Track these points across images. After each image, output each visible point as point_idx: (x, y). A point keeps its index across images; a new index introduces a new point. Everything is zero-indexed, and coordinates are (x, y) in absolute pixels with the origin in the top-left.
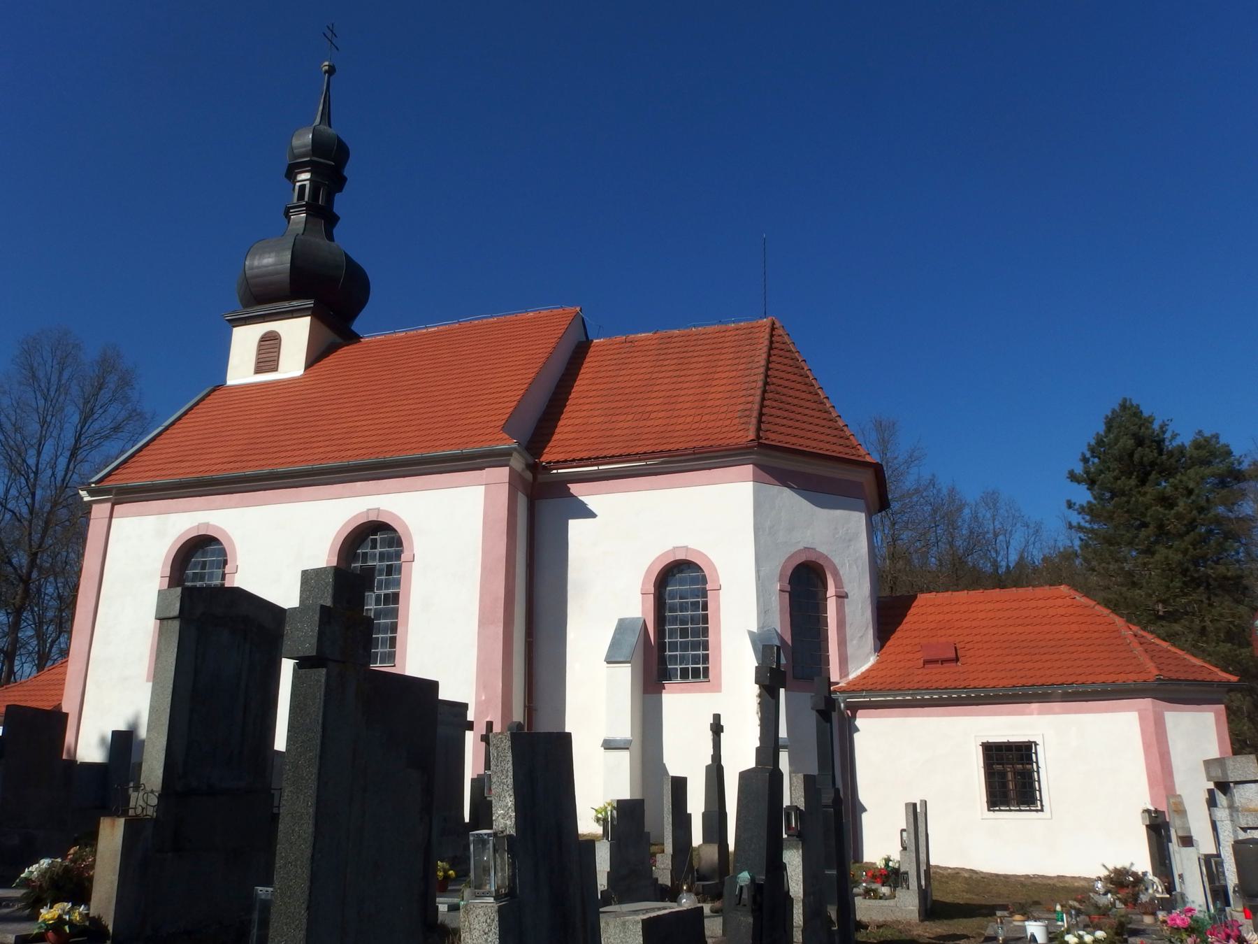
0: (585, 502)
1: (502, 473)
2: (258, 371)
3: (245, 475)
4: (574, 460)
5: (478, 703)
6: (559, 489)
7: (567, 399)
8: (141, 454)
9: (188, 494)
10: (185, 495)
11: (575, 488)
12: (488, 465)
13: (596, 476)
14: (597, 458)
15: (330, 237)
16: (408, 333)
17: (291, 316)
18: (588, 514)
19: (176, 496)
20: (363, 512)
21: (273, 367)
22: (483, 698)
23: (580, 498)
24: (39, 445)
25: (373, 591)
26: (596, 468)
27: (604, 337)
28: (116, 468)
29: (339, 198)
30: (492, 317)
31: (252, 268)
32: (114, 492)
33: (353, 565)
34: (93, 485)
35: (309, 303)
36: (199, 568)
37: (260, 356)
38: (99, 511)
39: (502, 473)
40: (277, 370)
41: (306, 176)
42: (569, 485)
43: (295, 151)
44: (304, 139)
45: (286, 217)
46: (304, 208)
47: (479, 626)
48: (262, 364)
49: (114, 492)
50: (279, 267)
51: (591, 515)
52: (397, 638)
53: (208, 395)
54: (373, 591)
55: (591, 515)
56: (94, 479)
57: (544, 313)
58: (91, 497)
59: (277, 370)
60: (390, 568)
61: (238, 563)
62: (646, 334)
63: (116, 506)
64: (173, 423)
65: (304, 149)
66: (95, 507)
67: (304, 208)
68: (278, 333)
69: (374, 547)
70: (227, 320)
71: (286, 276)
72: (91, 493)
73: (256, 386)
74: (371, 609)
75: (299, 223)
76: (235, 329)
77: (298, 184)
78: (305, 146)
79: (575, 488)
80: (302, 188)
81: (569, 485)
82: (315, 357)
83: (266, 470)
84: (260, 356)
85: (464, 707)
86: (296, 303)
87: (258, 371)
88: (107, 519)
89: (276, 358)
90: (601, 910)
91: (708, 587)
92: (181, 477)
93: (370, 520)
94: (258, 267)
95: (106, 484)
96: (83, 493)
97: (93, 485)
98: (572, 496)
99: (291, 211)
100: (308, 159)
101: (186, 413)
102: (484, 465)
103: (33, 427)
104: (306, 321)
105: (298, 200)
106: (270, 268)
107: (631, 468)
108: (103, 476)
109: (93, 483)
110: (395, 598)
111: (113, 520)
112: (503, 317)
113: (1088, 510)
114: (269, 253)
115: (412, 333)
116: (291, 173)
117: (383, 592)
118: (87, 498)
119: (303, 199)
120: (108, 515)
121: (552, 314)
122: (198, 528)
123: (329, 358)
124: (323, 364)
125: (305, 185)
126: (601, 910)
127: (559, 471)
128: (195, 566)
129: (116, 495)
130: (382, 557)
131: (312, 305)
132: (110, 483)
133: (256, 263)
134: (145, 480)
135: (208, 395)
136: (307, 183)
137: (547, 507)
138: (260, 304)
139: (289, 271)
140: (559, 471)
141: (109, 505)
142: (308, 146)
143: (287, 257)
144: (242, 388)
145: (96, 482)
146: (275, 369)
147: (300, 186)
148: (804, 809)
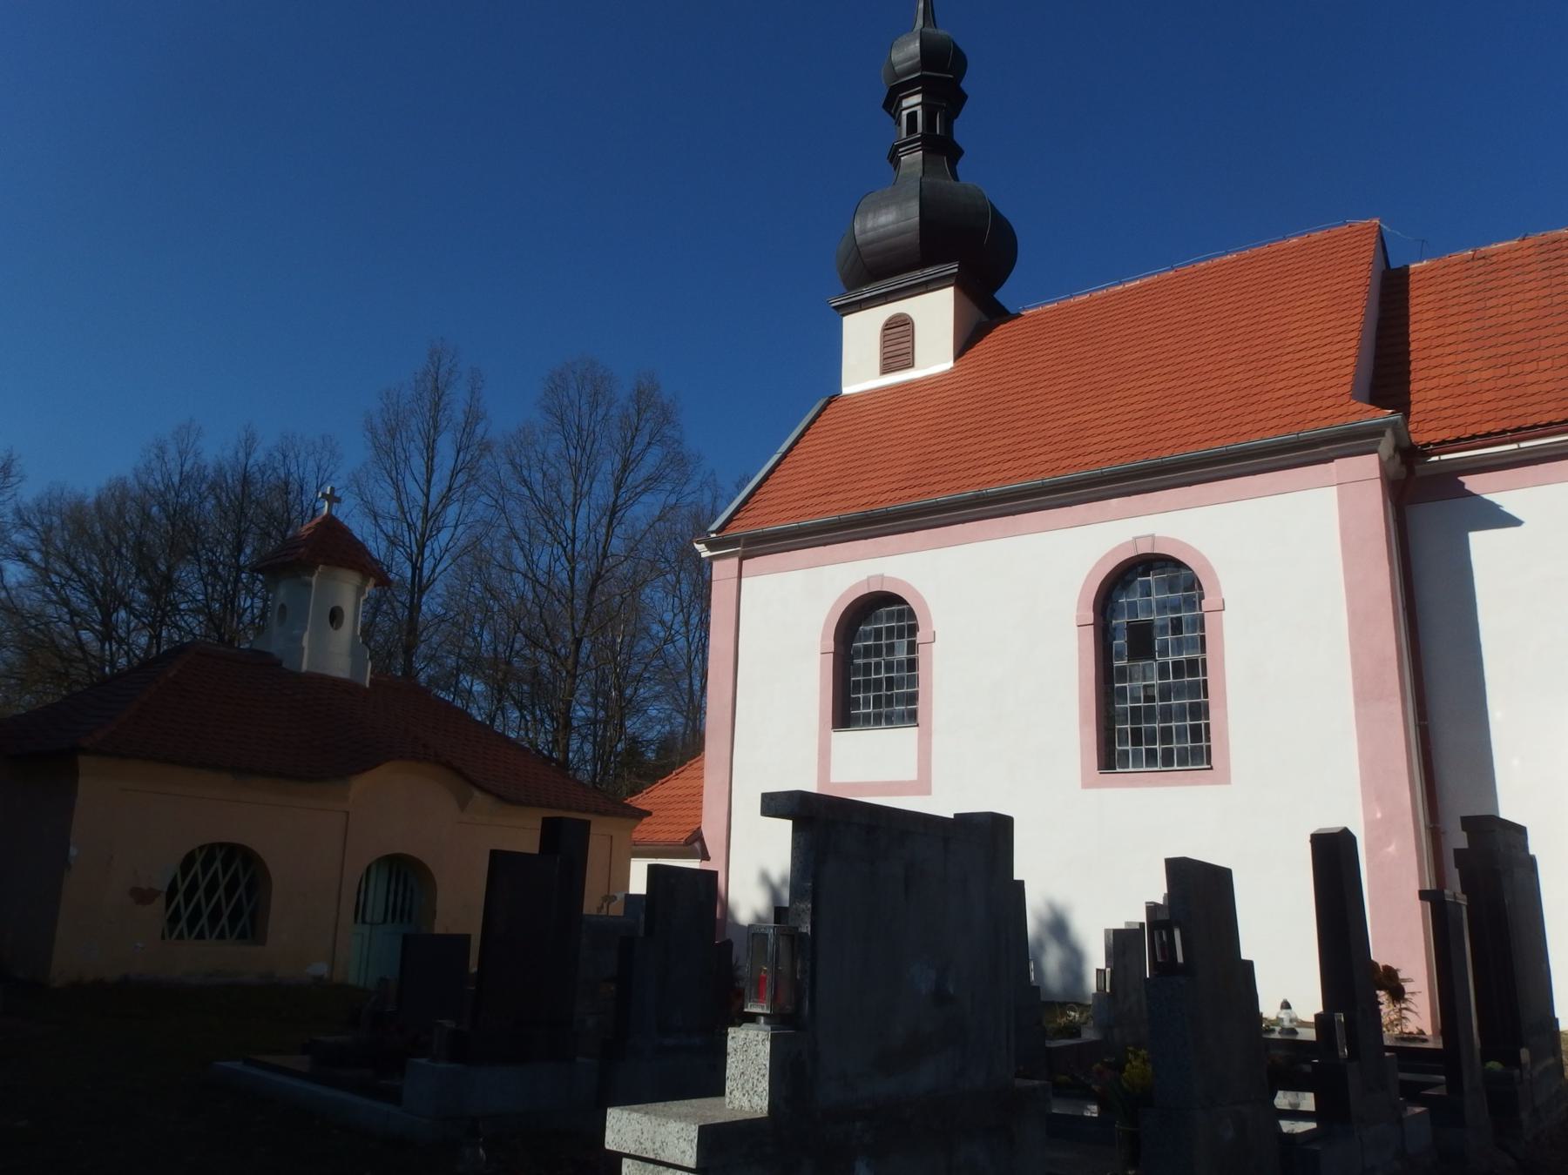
0: (1497, 503)
1: (1368, 466)
2: (886, 369)
3: (937, 502)
4: (1474, 437)
5: (1370, 825)
6: (1448, 485)
7: (1408, 353)
8: (761, 490)
9: (848, 537)
10: (833, 540)
11: (1472, 483)
12: (1336, 453)
13: (1510, 459)
14: (1519, 429)
15: (956, 178)
16: (1094, 294)
18: (1500, 519)
19: (794, 546)
20: (1127, 543)
21: (906, 362)
22: (1379, 815)
23: (1486, 497)
24: (574, 506)
25: (1153, 658)
26: (1514, 446)
27: (1427, 258)
28: (737, 511)
29: (959, 126)
30: (1227, 253)
31: (864, 232)
32: (742, 541)
33: (1114, 622)
34: (713, 535)
35: (953, 268)
36: (872, 639)
38: (723, 571)
39: (1368, 466)
41: (917, 99)
42: (1461, 478)
43: (896, 68)
44: (907, 51)
45: (891, 162)
46: (919, 143)
47: (1357, 704)
48: (890, 361)
49: (742, 541)
50: (902, 224)
51: (1511, 521)
53: (824, 408)
54: (1153, 658)
55: (1511, 521)
56: (714, 527)
57: (1317, 235)
58: (711, 551)
59: (913, 366)
60: (1177, 626)
61: (934, 629)
62: (1507, 243)
63: (744, 562)
64: (790, 449)
65: (910, 63)
66: (716, 564)
67: (919, 143)
68: (908, 316)
69: (1147, 592)
70: (834, 307)
71: (914, 236)
72: (711, 545)
73: (888, 390)
74: (1153, 685)
75: (914, 164)
76: (846, 319)
77: (905, 113)
78: (911, 58)
79: (1472, 483)
80: (912, 117)
81: (1461, 478)
82: (966, 341)
83: (970, 492)
85: (500, 861)
86: (931, 271)
87: (886, 369)
88: (736, 580)
89: (910, 350)
90: (1313, 1125)
92: (864, 509)
93: (1140, 553)
94: (874, 229)
95: (729, 533)
96: (700, 547)
97: (713, 535)
98: (1470, 494)
99: (900, 150)
100: (919, 74)
101: (802, 435)
102: (1331, 455)
103: (567, 489)
104: (948, 294)
105: (908, 134)
106: (890, 227)
107: (1560, 444)
108: (724, 523)
109: (712, 532)
110: (1195, 667)
111: (743, 580)
112: (1248, 251)
114: (887, 206)
115: (1100, 293)
116: (892, 103)
117: (1171, 659)
118: (706, 554)
120: (736, 574)
122: (869, 584)
123: (973, 350)
124: (978, 351)
125: (915, 112)
126: (1313, 1125)
127: (1444, 457)
128: (867, 636)
129: (744, 546)
130: (1163, 606)
131: (956, 270)
132: (731, 532)
133: (870, 224)
134: (825, 515)
135: (824, 408)
136: (919, 109)
137: (1426, 515)
138: (878, 281)
139: (918, 227)
140: (1444, 457)
141: (735, 560)
142: (917, 56)
143: (914, 208)
144: (868, 394)
145: (716, 532)
146: (910, 365)
147: (908, 115)
148: (1378, 992)
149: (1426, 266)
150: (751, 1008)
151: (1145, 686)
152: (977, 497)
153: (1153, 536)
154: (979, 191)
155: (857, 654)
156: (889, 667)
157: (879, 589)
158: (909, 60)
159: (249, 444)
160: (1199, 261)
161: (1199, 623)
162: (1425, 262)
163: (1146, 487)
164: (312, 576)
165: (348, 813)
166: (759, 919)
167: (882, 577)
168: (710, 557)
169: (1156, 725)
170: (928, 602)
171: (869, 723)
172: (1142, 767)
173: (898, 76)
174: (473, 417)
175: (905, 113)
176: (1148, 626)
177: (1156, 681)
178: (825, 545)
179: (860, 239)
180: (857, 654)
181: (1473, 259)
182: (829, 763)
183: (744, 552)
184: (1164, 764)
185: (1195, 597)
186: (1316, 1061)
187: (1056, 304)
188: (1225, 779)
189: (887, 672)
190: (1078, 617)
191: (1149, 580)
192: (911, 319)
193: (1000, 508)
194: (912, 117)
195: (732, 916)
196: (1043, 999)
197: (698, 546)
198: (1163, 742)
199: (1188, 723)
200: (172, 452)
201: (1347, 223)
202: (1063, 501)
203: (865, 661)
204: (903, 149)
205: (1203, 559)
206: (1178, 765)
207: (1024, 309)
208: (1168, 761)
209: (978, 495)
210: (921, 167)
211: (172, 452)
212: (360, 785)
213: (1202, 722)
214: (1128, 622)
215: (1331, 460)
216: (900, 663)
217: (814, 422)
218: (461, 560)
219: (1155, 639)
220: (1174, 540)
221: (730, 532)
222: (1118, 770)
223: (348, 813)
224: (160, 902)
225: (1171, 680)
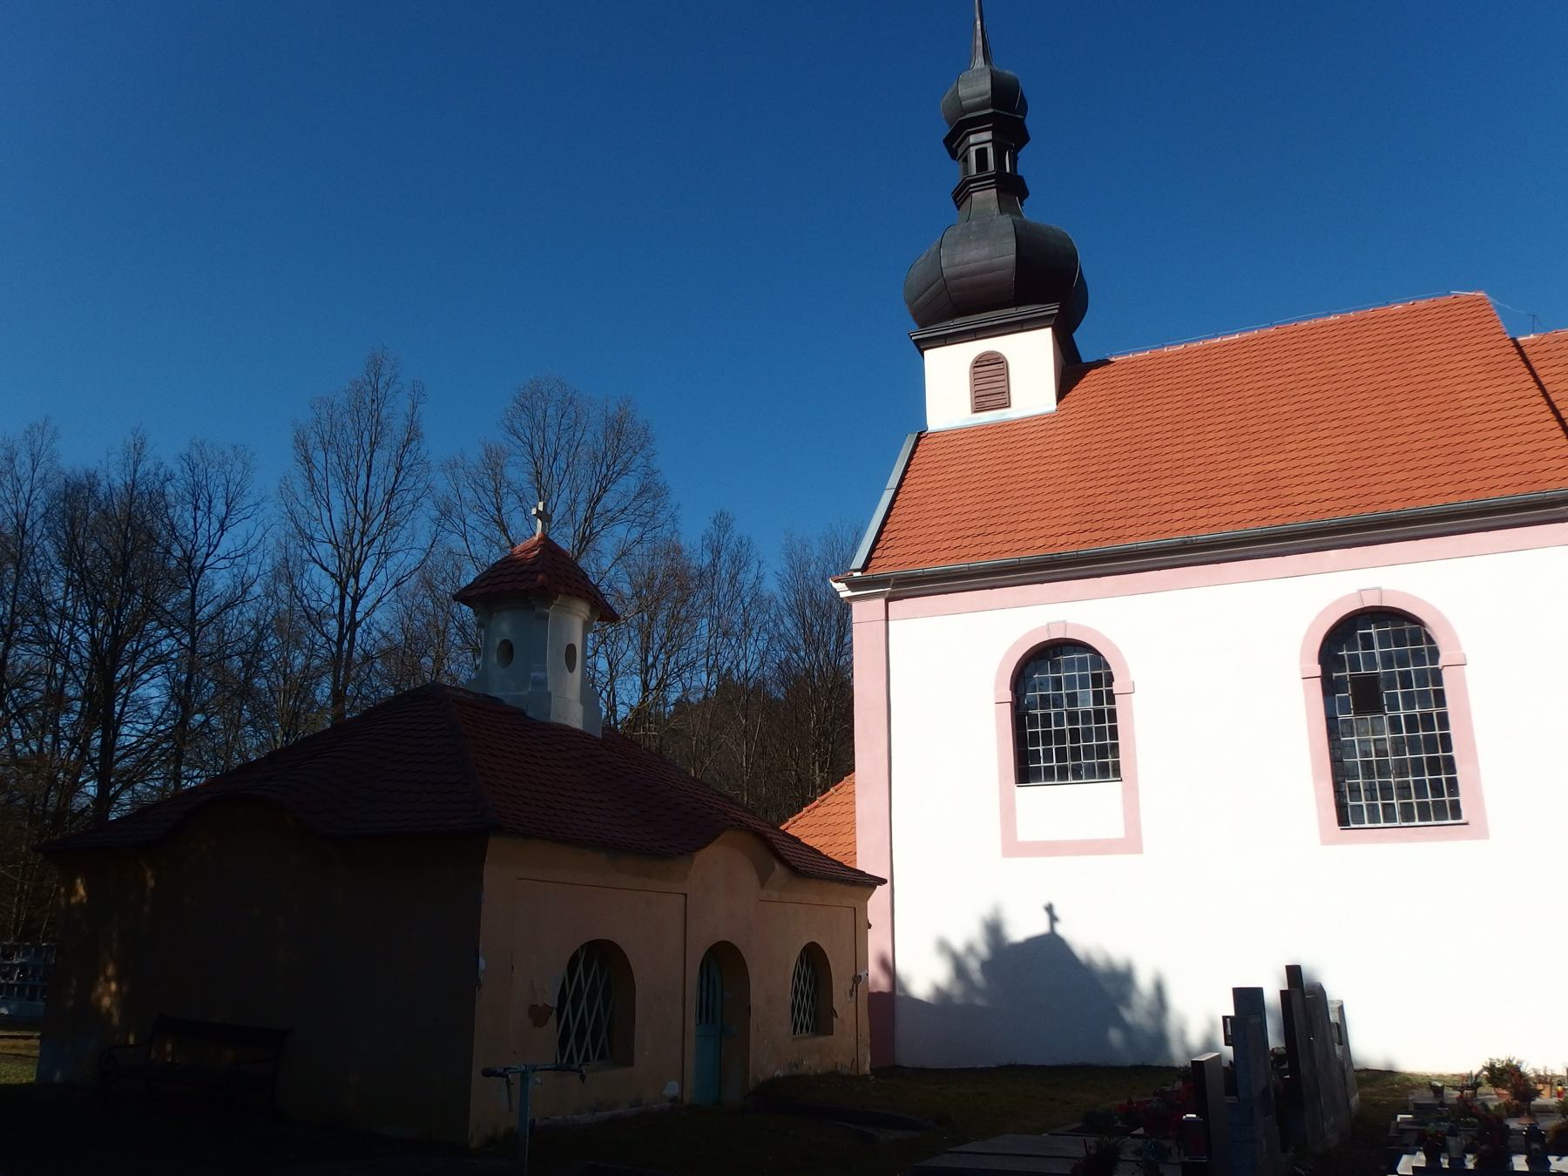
2: (978, 408)
17: (1020, 329)
21: (1002, 402)
37: (978, 388)
38: (866, 613)
40: (1009, 406)
41: (987, 136)
44: (975, 86)
46: (993, 180)
52: (1458, 779)
54: (1383, 712)
57: (1422, 304)
59: (1009, 406)
61: (1132, 678)
65: (978, 99)
66: (855, 605)
67: (993, 180)
72: (853, 584)
84: (978, 388)
87: (978, 408)
91: (1116, 688)
96: (839, 586)
99: (972, 185)
111: (890, 622)
113: (588, 617)
118: (843, 591)
119: (986, 168)
120: (884, 617)
121: (1434, 305)
129: (894, 586)
131: (1057, 311)
133: (958, 259)
141: (882, 601)
146: (1007, 405)
149: (1534, 340)
151: (1375, 740)
152: (1185, 543)
154: (1066, 234)
155: (1033, 706)
156: (1073, 718)
158: (977, 97)
159: (137, 452)
160: (1299, 320)
161: (1437, 677)
163: (1372, 539)
164: (549, 608)
165: (686, 895)
166: (938, 991)
167: (1065, 624)
168: (850, 598)
169: (1391, 780)
171: (1052, 778)
173: (966, 111)
174: (414, 433)
175: (973, 149)
176: (1374, 679)
177: (1387, 735)
178: (991, 588)
179: (947, 273)
180: (1033, 706)
182: (1014, 821)
183: (890, 593)
185: (1423, 651)
188: (1483, 834)
189: (1070, 723)
190: (1303, 670)
191: (1371, 633)
192: (1004, 358)
193: (1207, 556)
194: (981, 154)
195: (904, 989)
196: (1356, 1067)
197: (836, 586)
198: (1400, 797)
200: (24, 458)
201: (1451, 295)
202: (1276, 551)
203: (1043, 711)
204: (975, 185)
205: (1439, 613)
206: (1420, 820)
207: (1112, 356)
208: (1408, 817)
209: (1185, 542)
210: (997, 204)
211: (24, 458)
212: (703, 856)
214: (1350, 675)
216: (1086, 714)
217: (913, 459)
219: (1382, 693)
221: (875, 571)
222: (1353, 826)
223: (686, 895)
224: (553, 1019)
225: (1404, 734)
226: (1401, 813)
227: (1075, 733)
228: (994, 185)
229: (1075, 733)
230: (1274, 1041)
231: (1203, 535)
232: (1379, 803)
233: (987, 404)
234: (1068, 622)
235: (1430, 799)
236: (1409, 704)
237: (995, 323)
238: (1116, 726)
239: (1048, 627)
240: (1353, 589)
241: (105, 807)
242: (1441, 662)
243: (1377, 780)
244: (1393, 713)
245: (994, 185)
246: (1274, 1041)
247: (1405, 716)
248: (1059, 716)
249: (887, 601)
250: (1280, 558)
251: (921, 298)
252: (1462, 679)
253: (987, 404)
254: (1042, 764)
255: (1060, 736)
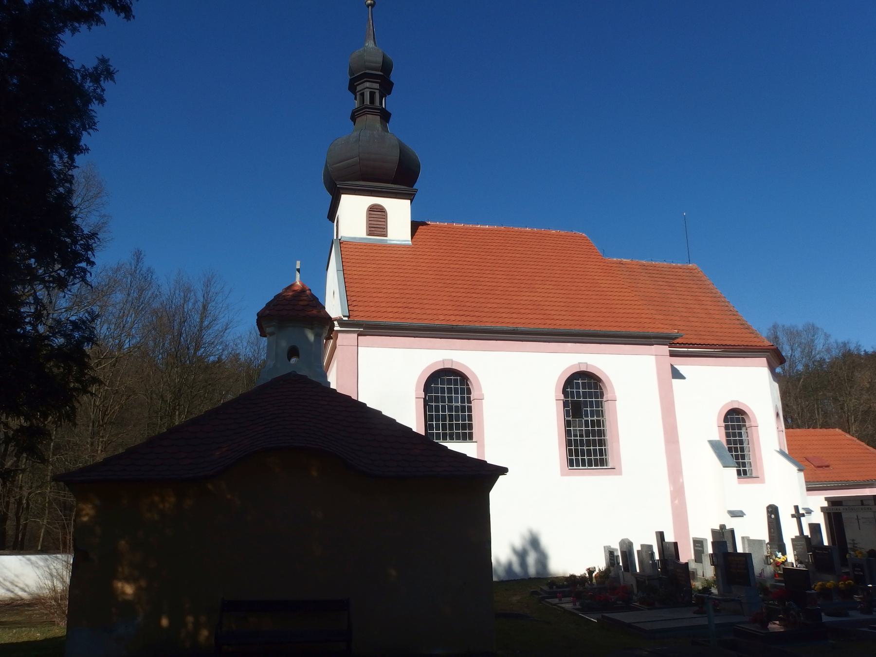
2: (370, 233)
20: (575, 365)
46: (379, 111)
66: (340, 335)
67: (379, 111)
91: (472, 397)
99: (356, 114)
102: (653, 343)
146: (386, 236)
150: (578, 604)
151: (579, 430)
153: (586, 363)
157: (450, 367)
162: (487, 227)
167: (452, 361)
169: (585, 448)
170: (478, 376)
172: (598, 466)
181: (620, 263)
184: (589, 466)
186: (871, 586)
187: (446, 224)
192: (385, 210)
199: (598, 448)
208: (590, 465)
213: (603, 448)
215: (653, 345)
216: (457, 407)
218: (96, 295)
220: (595, 367)
226: (588, 463)
227: (451, 416)
228: (379, 114)
229: (451, 416)
230: (657, 557)
231: (521, 327)
232: (580, 458)
233: (375, 232)
234: (454, 360)
235: (598, 457)
236: (592, 416)
237: (384, 190)
238: (472, 415)
239: (443, 361)
240: (441, 359)
241: (790, 420)
242: (604, 399)
243: (579, 448)
244: (593, 419)
245: (379, 114)
246: (657, 557)
247: (591, 420)
248: (443, 407)
249: (358, 335)
250: (467, 340)
251: (342, 163)
252: (615, 406)
253: (375, 232)
254: (435, 431)
255: (444, 418)
